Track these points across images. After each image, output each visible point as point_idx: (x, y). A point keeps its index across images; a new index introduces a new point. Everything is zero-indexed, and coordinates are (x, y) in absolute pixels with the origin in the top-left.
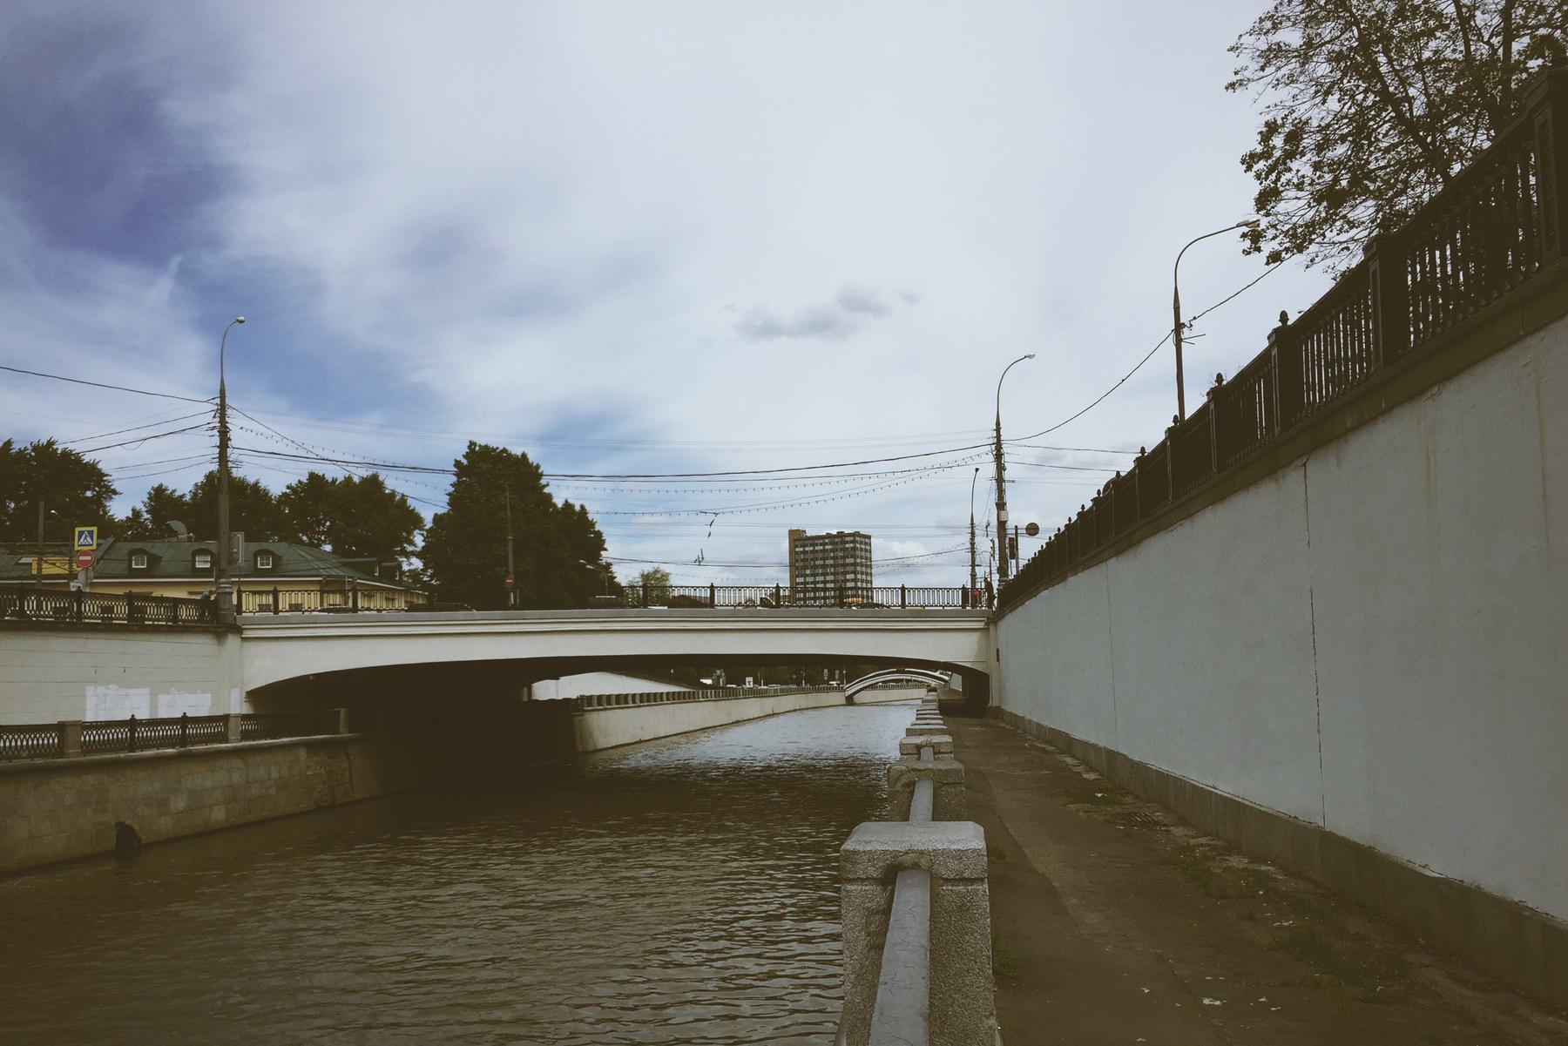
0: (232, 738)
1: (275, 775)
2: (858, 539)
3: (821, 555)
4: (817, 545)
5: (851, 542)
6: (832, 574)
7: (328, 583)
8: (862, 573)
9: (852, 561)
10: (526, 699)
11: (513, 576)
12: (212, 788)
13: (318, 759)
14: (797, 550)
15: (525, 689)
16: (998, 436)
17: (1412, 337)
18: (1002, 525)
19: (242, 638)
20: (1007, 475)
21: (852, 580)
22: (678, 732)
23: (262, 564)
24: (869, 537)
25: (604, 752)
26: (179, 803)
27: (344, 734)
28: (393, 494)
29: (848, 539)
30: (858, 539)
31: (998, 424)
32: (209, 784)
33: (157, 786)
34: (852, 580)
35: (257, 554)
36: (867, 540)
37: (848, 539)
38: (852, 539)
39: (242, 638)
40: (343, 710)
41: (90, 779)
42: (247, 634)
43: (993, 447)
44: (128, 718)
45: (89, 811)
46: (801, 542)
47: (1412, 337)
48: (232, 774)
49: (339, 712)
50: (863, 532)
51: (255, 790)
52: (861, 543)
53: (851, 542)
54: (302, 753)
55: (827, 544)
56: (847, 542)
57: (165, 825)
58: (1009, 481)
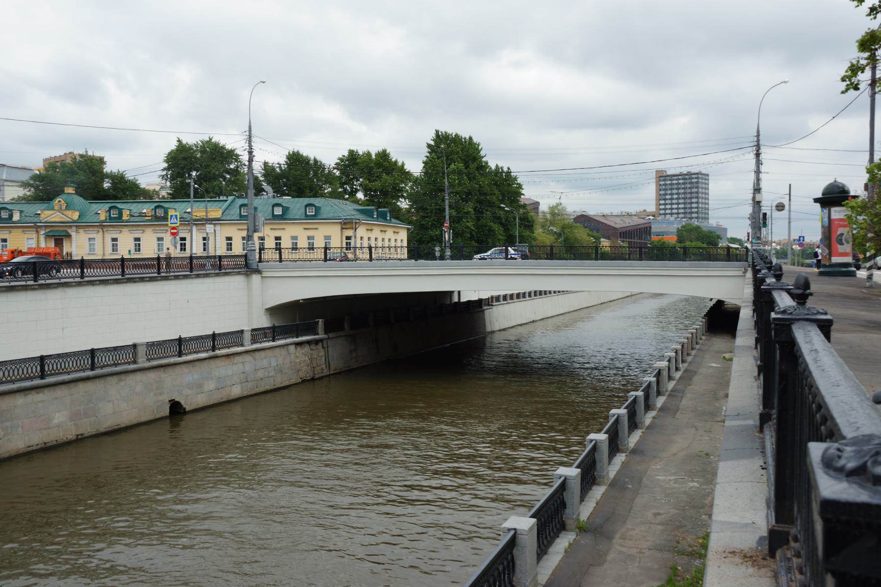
0: (245, 344)
1: (274, 364)
2: (700, 176)
3: (675, 186)
4: (673, 180)
5: (696, 178)
6: (683, 198)
7: (345, 223)
8: (702, 198)
9: (695, 190)
10: (449, 303)
11: (448, 222)
12: (232, 374)
13: (303, 351)
14: (661, 183)
15: (118, 568)
16: (758, 141)
17: (773, 332)
18: (757, 204)
19: (262, 277)
20: (763, 168)
21: (696, 208)
22: (570, 310)
23: (309, 212)
24: (708, 175)
25: (513, 331)
26: (211, 385)
27: (321, 336)
28: (396, 162)
29: (693, 176)
30: (700, 176)
31: (758, 132)
32: (230, 372)
33: (196, 376)
34: (696, 208)
35: (307, 206)
36: (707, 177)
37: (693, 176)
38: (696, 176)
39: (262, 277)
40: (320, 320)
41: (152, 375)
42: (265, 274)
43: (754, 148)
44: (177, 337)
45: (152, 394)
46: (663, 178)
47: (773, 332)
48: (247, 365)
49: (318, 321)
50: (704, 172)
51: (260, 374)
52: (702, 179)
53: (696, 178)
54: (292, 348)
55: (680, 179)
56: (693, 178)
57: (201, 400)
58: (765, 173)
